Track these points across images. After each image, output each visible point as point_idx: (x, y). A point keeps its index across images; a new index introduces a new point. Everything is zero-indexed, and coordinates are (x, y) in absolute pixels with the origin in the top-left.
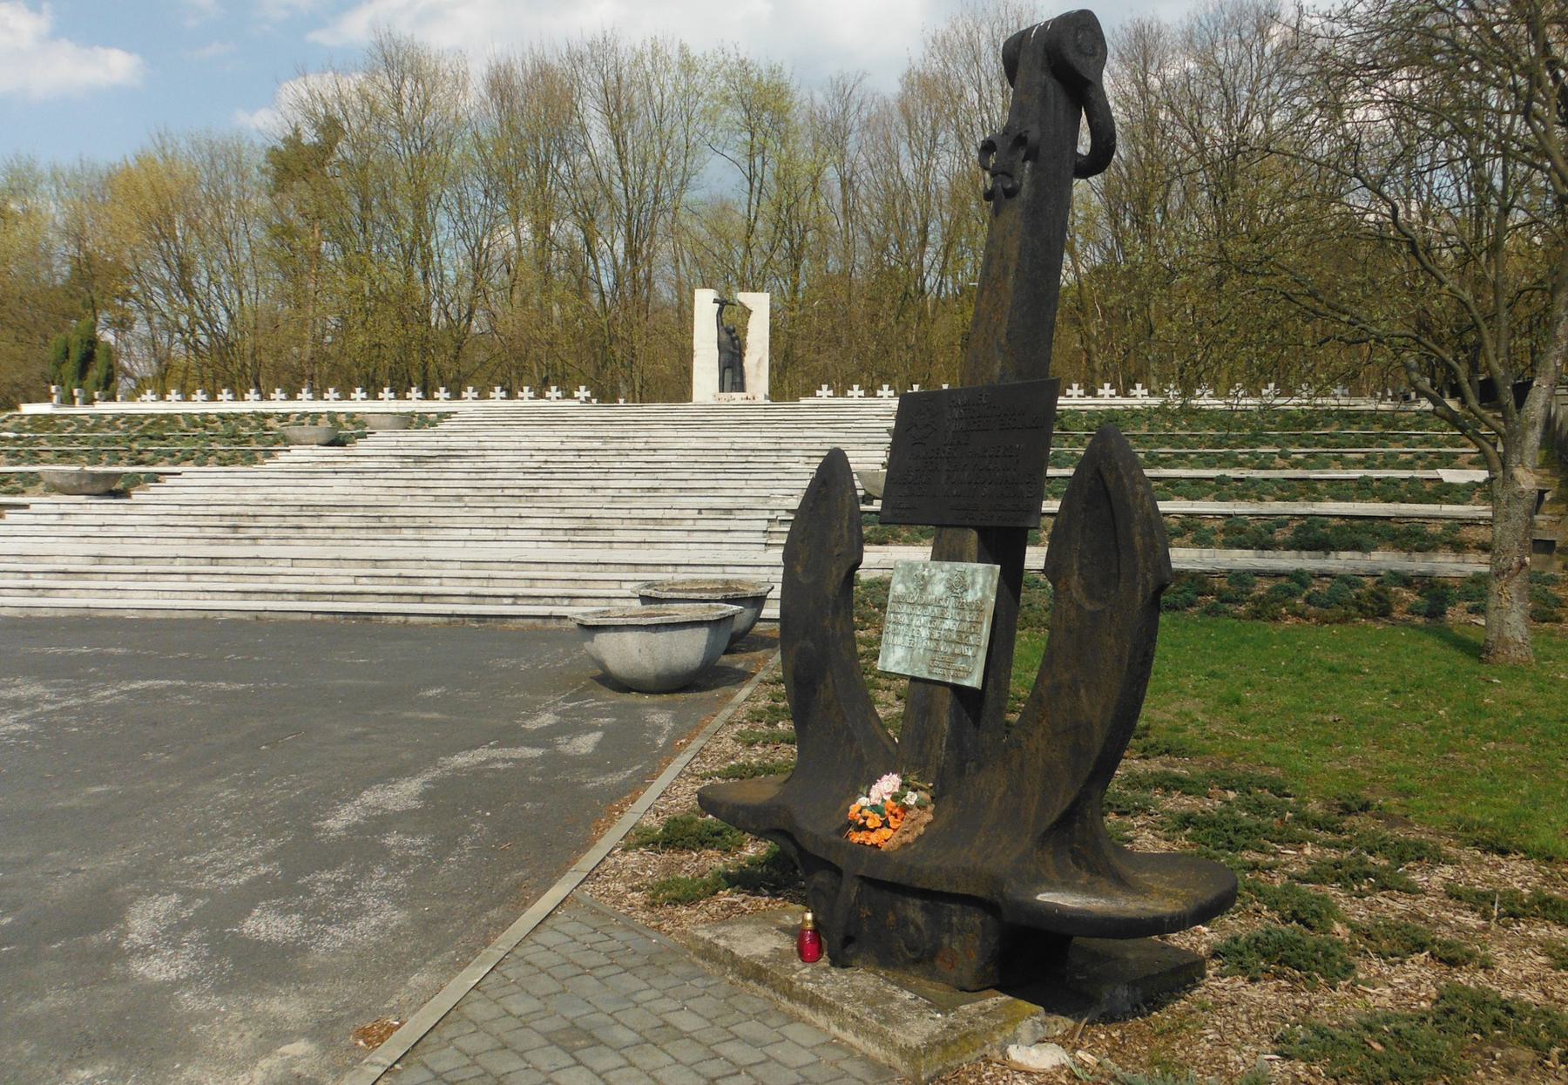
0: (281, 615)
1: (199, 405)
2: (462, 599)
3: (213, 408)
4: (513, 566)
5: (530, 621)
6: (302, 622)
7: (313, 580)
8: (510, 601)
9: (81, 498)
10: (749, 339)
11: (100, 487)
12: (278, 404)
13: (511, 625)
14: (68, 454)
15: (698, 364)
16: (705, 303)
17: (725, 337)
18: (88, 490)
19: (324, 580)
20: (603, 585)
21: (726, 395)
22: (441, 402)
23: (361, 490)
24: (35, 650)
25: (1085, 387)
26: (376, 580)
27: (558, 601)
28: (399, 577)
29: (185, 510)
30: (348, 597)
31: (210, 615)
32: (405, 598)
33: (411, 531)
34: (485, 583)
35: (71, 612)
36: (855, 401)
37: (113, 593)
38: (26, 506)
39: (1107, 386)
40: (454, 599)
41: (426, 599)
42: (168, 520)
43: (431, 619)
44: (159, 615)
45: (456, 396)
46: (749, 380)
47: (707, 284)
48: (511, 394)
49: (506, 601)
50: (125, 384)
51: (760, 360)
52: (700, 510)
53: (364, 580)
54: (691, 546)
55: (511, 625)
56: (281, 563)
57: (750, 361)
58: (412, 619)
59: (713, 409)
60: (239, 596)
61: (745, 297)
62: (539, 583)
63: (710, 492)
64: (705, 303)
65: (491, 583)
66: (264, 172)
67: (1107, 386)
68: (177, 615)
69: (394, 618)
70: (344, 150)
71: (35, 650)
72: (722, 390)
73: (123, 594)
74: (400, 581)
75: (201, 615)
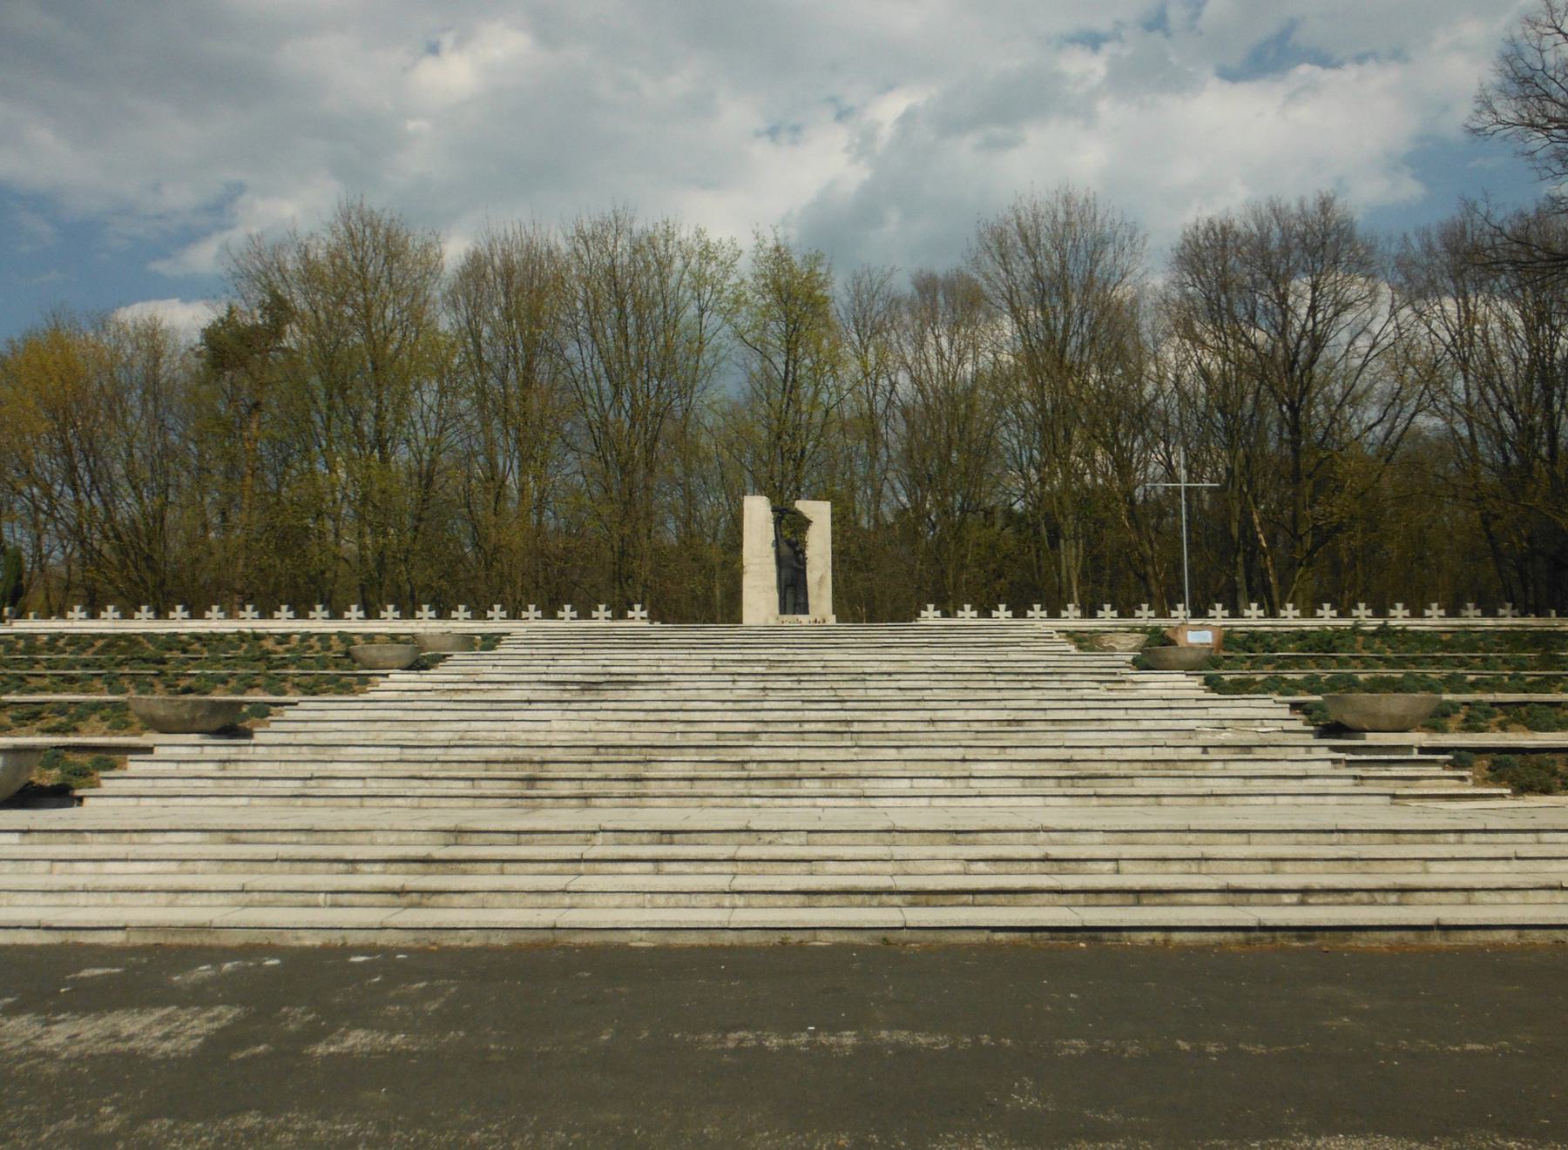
0: (930, 935)
1: (109, 623)
2: (1209, 898)
3: (198, 626)
4: (1191, 837)
5: (1393, 935)
6: (971, 947)
7: (889, 867)
8: (1294, 898)
9: (194, 738)
10: (809, 553)
11: (218, 722)
12: (354, 623)
13: (1360, 941)
14: (72, 680)
15: (748, 582)
16: (757, 512)
17: (785, 549)
18: (203, 725)
19: (910, 867)
20: (1395, 866)
21: (785, 617)
22: (496, 622)
23: (593, 726)
24: (921, 1040)
25: (1446, 608)
26: (1003, 867)
27: (1379, 897)
28: (1046, 859)
29: (410, 754)
30: (1002, 898)
31: (795, 937)
32: (1107, 898)
33: (817, 783)
34: (1194, 867)
35: (517, 936)
36: (602, 623)
37: (556, 899)
38: (148, 750)
39: (1435, 605)
40: (1196, 898)
41: (1145, 899)
42: (425, 770)
43: (1214, 937)
44: (693, 939)
45: (514, 615)
46: (812, 601)
47: (761, 489)
48: (620, 614)
49: (1286, 898)
50: (37, 596)
51: (822, 578)
52: (1205, 748)
53: (981, 866)
54: (1281, 800)
55: (1360, 941)
56: (786, 838)
57: (812, 576)
58: (1177, 937)
59: (771, 630)
60: (800, 899)
61: (803, 506)
62: (1288, 866)
63: (1094, 726)
64: (757, 512)
65: (1205, 867)
66: (199, 355)
67: (1435, 605)
68: (728, 938)
69: (1144, 937)
70: (292, 337)
71: (921, 1040)
72: (783, 610)
73: (577, 899)
74: (1045, 866)
75: (776, 938)
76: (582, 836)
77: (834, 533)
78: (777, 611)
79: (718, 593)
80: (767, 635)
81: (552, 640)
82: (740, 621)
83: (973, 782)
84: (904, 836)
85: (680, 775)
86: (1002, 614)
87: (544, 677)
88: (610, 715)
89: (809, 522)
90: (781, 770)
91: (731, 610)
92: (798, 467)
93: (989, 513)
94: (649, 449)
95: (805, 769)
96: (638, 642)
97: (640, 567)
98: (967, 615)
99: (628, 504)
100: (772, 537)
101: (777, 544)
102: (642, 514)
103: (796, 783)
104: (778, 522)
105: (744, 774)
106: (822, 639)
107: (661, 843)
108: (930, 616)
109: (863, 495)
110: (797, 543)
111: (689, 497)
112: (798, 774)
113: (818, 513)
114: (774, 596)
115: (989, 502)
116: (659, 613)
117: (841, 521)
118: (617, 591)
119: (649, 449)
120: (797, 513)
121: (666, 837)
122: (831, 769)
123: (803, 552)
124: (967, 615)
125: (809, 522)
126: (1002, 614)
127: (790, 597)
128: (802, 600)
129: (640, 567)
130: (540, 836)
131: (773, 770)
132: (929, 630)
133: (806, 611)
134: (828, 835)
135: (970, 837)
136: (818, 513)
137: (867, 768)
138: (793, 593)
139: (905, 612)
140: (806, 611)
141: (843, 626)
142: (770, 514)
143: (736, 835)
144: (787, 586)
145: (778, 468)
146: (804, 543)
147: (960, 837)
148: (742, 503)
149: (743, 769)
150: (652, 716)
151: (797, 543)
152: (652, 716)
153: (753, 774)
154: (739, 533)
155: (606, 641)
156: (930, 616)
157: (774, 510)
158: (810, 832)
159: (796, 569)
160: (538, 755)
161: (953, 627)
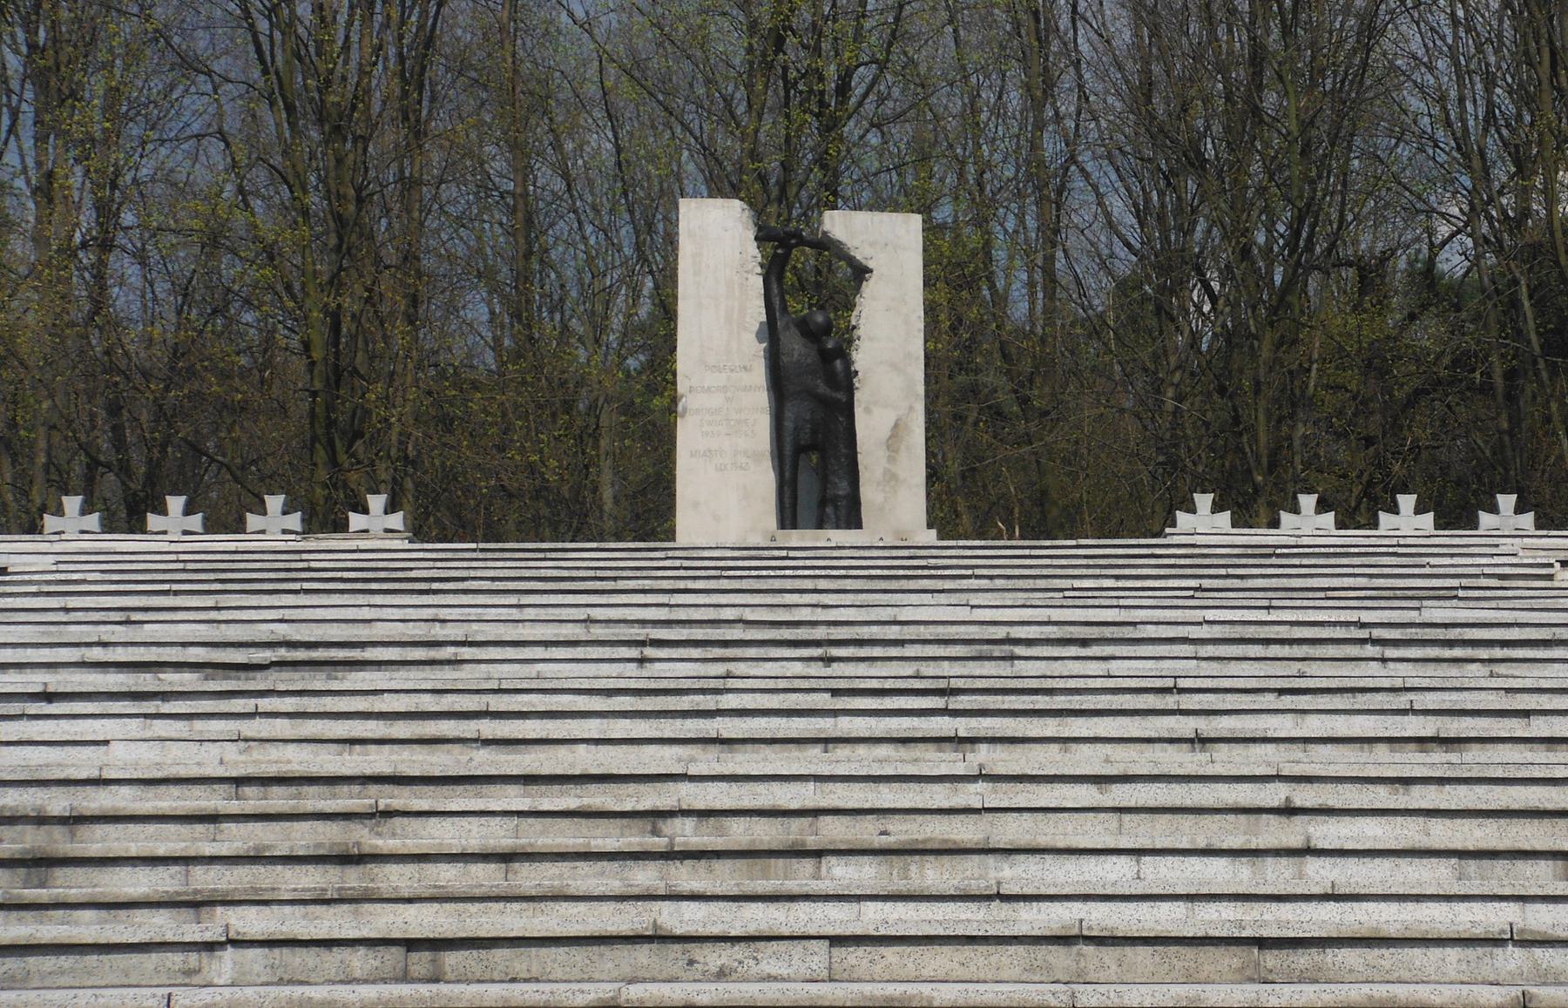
10: (862, 358)
16: (716, 244)
17: (795, 346)
46: (869, 493)
47: (720, 185)
51: (898, 430)
61: (840, 224)
64: (716, 244)
72: (788, 517)
76: (175, 959)
77: (930, 309)
78: (772, 522)
79: (607, 494)
80: (736, 566)
81: (124, 579)
82: (671, 535)
83: (1313, 865)
84: (1109, 954)
85: (474, 844)
86: (1407, 521)
87: (97, 654)
88: (282, 727)
89: (861, 272)
90: (765, 833)
91: (649, 510)
92: (830, 126)
93: (1370, 274)
94: (413, 78)
95: (834, 831)
96: (372, 580)
97: (387, 401)
98: (1308, 523)
99: (347, 233)
100: (756, 312)
101: (771, 332)
102: (391, 255)
103: (808, 865)
104: (774, 271)
105: (659, 843)
106: (901, 570)
107: (405, 978)
108: (1203, 523)
109: (1013, 223)
110: (827, 329)
111: (527, 223)
112: (812, 842)
113: (888, 249)
114: (764, 480)
115: (1366, 242)
116: (440, 514)
117: (953, 278)
118: (323, 474)
119: (413, 78)
120: (826, 245)
121: (420, 962)
122: (903, 831)
123: (843, 352)
124: (1308, 523)
125: (861, 272)
126: (1407, 521)
127: (807, 485)
128: (843, 488)
129: (387, 401)
130: (49, 963)
131: (740, 833)
132: (1199, 559)
133: (853, 519)
134: (891, 953)
135: (1303, 959)
136: (888, 249)
137: (1011, 830)
138: (815, 462)
139: (1142, 511)
140: (853, 519)
141: (967, 550)
142: (752, 249)
143: (622, 952)
144: (800, 450)
145: (770, 128)
146: (848, 338)
147: (1271, 959)
148: (672, 222)
149: (655, 832)
150: (401, 729)
151: (827, 329)
152: (401, 729)
153: (680, 843)
154: (667, 311)
155: (288, 577)
156: (1203, 523)
157: (763, 236)
158: (837, 941)
159: (823, 401)
160: (58, 802)
161: (1270, 552)
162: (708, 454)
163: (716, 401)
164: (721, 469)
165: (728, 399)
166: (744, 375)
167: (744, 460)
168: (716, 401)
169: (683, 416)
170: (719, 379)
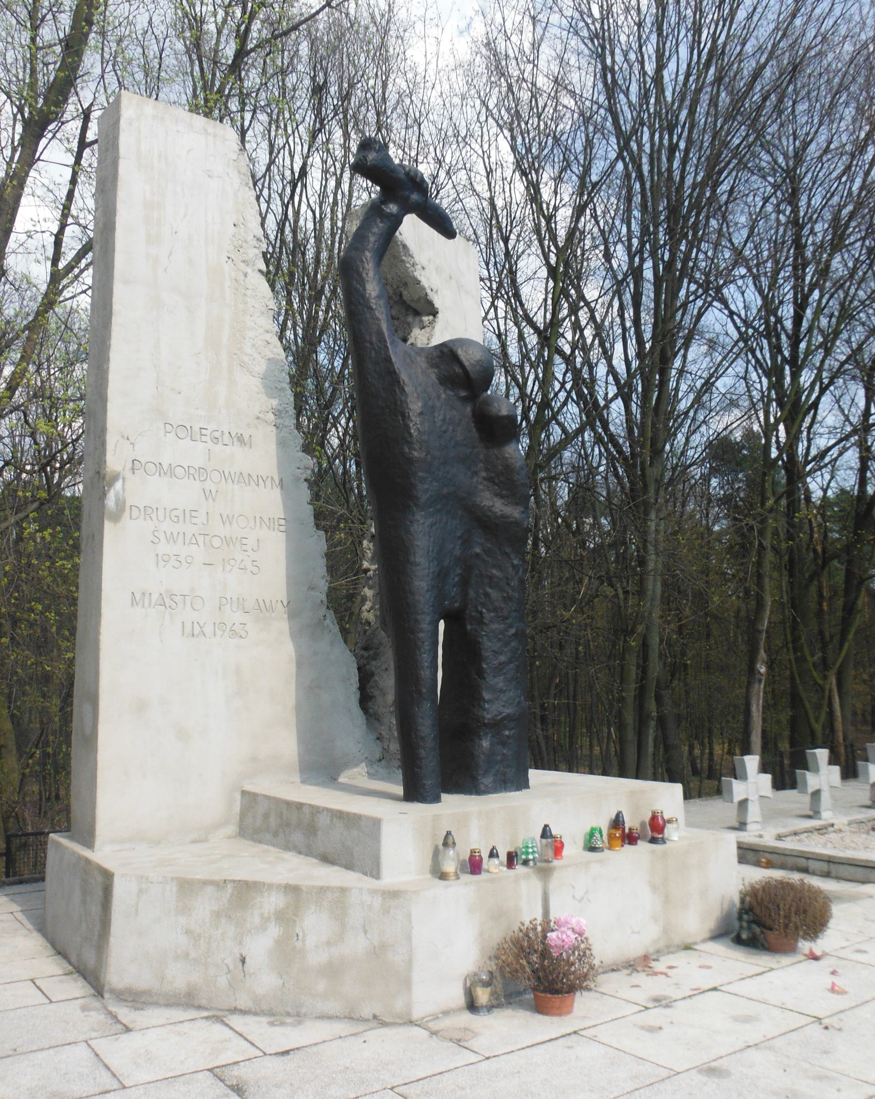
162: (167, 601)
163: (184, 494)
164: (194, 632)
165: (207, 495)
166: (236, 449)
167: (238, 617)
168: (184, 494)
169: (116, 517)
170: (194, 453)
